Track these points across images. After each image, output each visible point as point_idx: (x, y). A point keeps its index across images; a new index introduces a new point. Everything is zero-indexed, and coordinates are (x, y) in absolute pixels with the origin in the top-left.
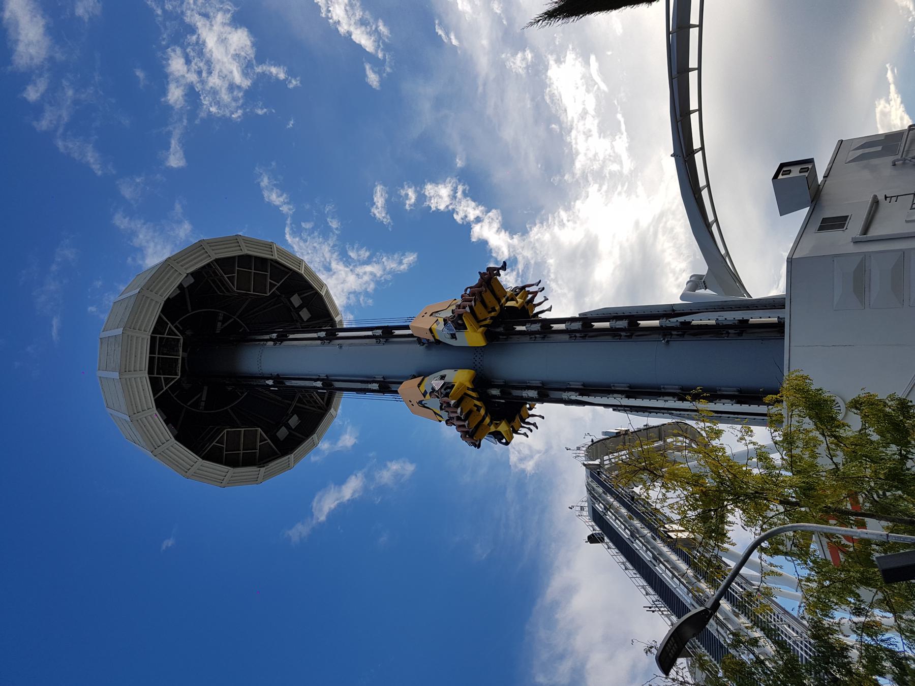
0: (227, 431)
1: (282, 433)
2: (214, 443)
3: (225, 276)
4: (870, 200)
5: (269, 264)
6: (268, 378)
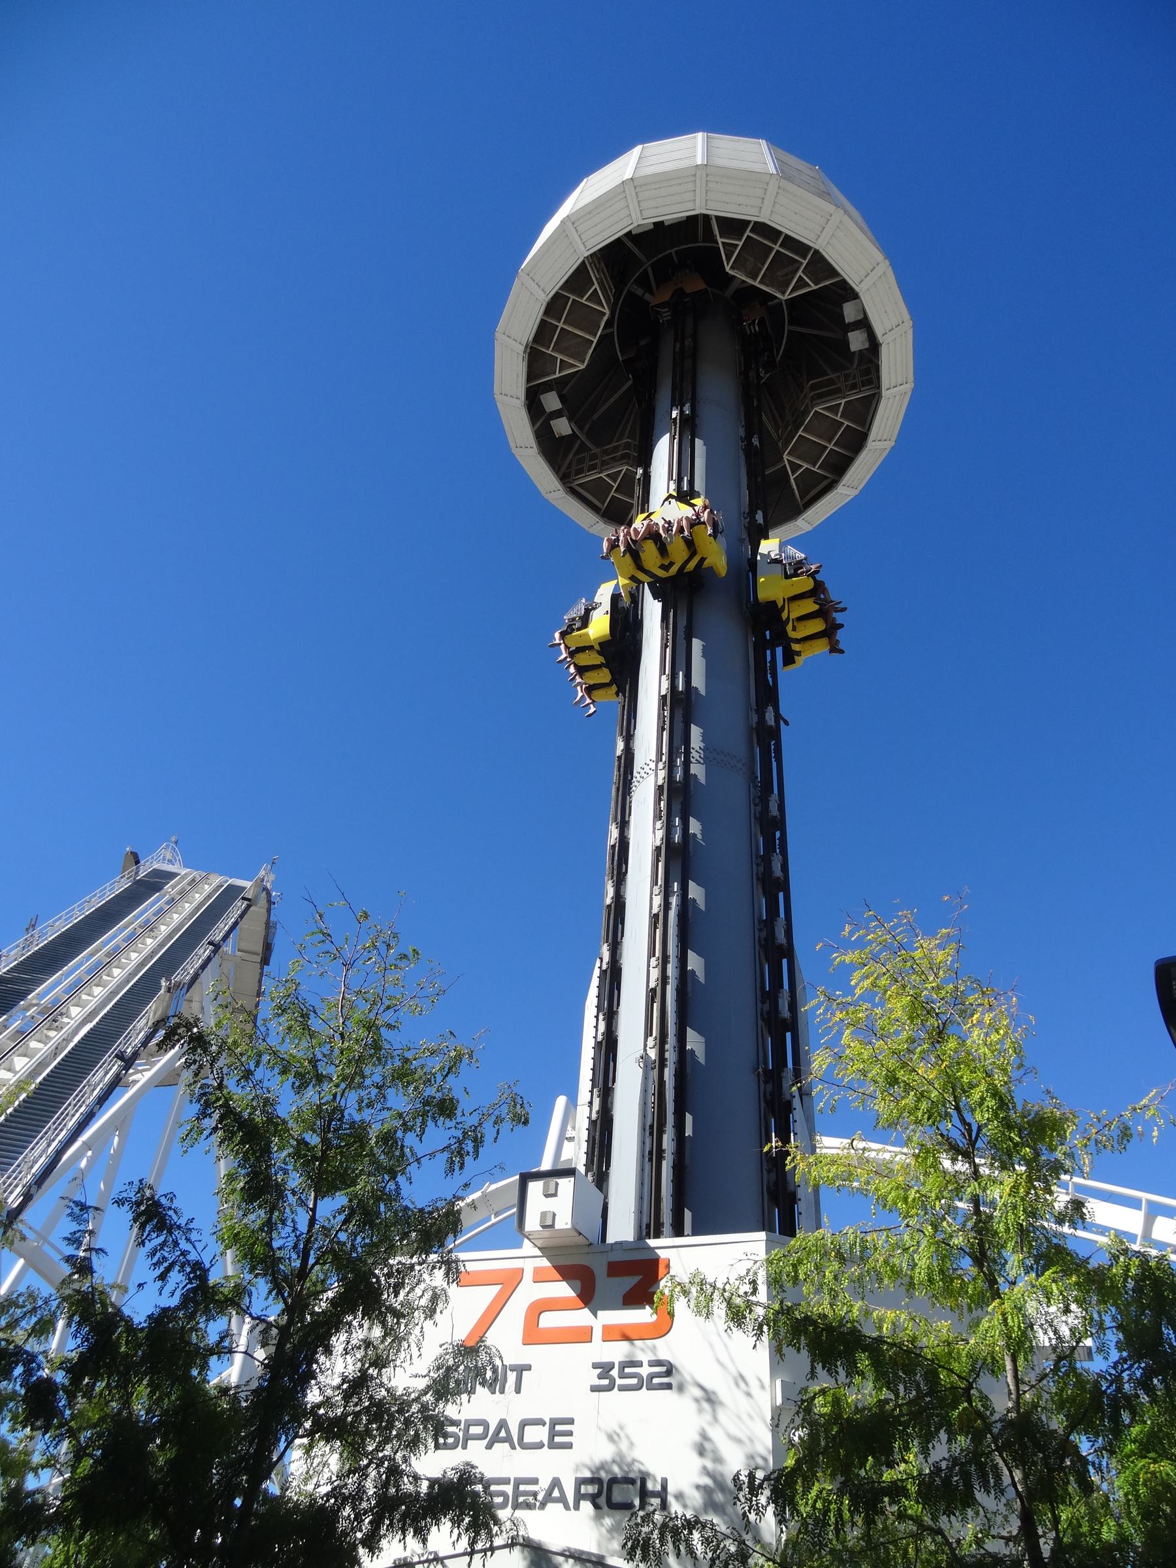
0: (605, 314)
1: (551, 401)
2: (596, 285)
3: (843, 401)
4: (476, 1465)
5: (828, 476)
6: (693, 409)
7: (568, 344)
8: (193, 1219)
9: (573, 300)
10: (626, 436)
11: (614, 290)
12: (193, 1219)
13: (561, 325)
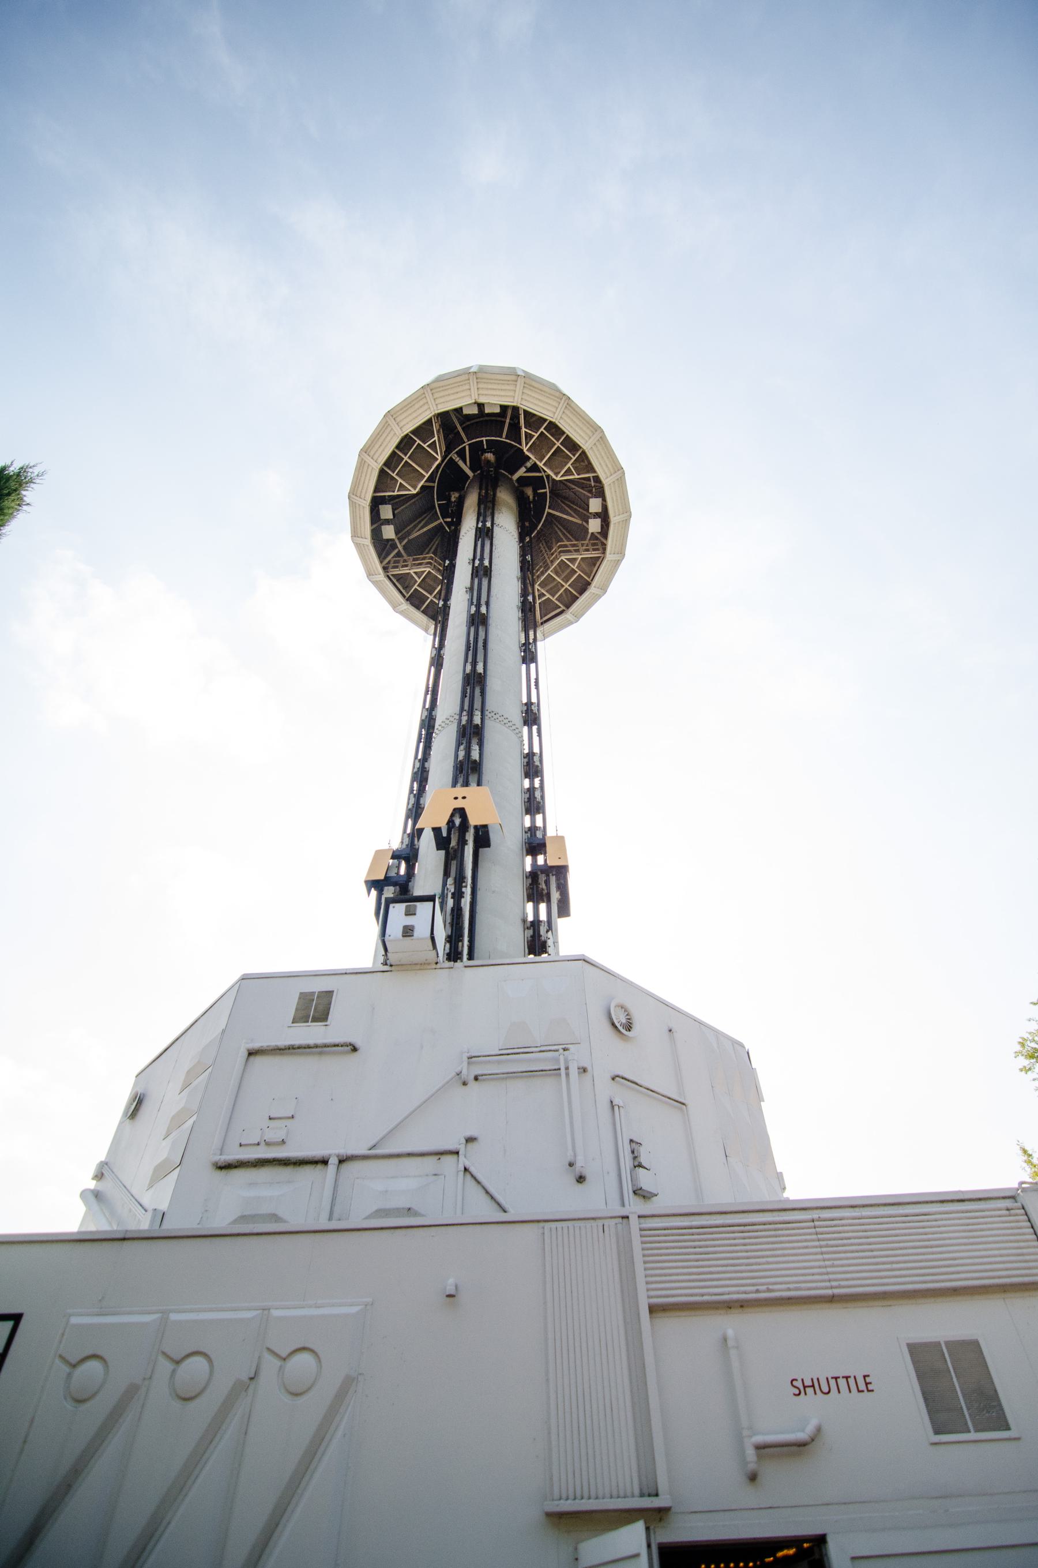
0: (437, 459)
2: (436, 438)
7: (408, 473)
8: (1021, 1070)
9: (419, 444)
10: (431, 552)
11: (443, 450)
12: (1021, 1070)
13: (406, 458)
